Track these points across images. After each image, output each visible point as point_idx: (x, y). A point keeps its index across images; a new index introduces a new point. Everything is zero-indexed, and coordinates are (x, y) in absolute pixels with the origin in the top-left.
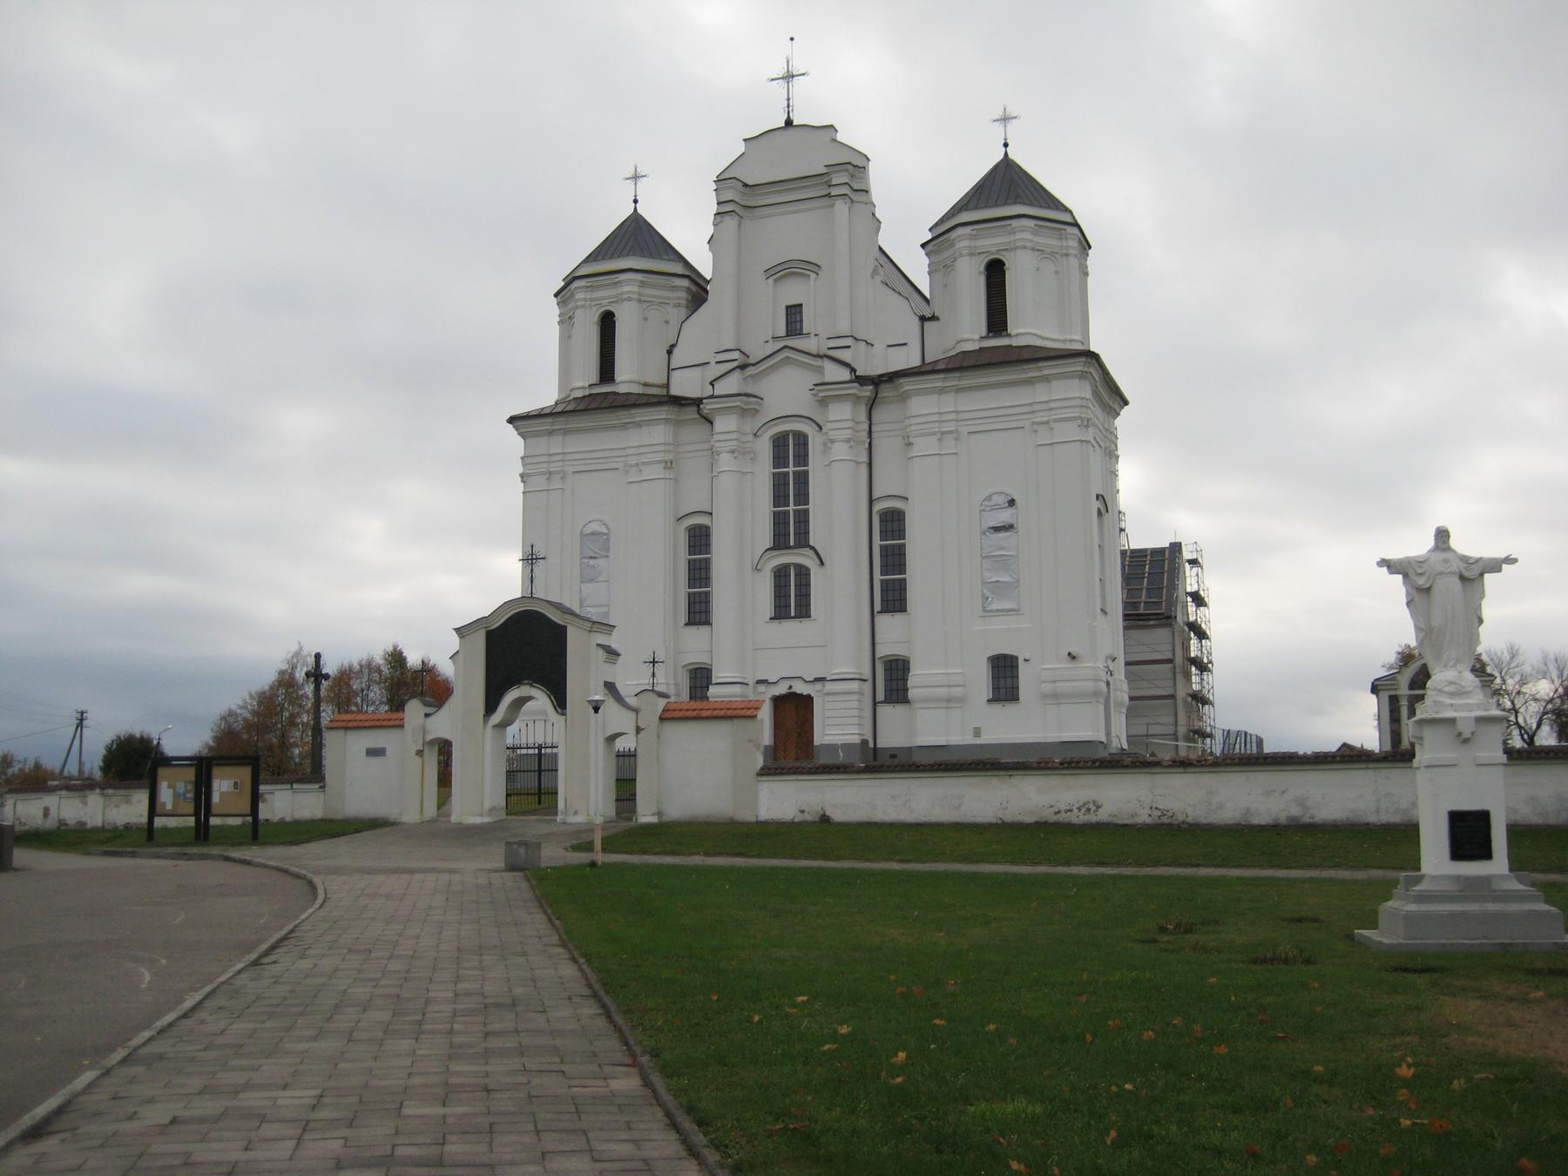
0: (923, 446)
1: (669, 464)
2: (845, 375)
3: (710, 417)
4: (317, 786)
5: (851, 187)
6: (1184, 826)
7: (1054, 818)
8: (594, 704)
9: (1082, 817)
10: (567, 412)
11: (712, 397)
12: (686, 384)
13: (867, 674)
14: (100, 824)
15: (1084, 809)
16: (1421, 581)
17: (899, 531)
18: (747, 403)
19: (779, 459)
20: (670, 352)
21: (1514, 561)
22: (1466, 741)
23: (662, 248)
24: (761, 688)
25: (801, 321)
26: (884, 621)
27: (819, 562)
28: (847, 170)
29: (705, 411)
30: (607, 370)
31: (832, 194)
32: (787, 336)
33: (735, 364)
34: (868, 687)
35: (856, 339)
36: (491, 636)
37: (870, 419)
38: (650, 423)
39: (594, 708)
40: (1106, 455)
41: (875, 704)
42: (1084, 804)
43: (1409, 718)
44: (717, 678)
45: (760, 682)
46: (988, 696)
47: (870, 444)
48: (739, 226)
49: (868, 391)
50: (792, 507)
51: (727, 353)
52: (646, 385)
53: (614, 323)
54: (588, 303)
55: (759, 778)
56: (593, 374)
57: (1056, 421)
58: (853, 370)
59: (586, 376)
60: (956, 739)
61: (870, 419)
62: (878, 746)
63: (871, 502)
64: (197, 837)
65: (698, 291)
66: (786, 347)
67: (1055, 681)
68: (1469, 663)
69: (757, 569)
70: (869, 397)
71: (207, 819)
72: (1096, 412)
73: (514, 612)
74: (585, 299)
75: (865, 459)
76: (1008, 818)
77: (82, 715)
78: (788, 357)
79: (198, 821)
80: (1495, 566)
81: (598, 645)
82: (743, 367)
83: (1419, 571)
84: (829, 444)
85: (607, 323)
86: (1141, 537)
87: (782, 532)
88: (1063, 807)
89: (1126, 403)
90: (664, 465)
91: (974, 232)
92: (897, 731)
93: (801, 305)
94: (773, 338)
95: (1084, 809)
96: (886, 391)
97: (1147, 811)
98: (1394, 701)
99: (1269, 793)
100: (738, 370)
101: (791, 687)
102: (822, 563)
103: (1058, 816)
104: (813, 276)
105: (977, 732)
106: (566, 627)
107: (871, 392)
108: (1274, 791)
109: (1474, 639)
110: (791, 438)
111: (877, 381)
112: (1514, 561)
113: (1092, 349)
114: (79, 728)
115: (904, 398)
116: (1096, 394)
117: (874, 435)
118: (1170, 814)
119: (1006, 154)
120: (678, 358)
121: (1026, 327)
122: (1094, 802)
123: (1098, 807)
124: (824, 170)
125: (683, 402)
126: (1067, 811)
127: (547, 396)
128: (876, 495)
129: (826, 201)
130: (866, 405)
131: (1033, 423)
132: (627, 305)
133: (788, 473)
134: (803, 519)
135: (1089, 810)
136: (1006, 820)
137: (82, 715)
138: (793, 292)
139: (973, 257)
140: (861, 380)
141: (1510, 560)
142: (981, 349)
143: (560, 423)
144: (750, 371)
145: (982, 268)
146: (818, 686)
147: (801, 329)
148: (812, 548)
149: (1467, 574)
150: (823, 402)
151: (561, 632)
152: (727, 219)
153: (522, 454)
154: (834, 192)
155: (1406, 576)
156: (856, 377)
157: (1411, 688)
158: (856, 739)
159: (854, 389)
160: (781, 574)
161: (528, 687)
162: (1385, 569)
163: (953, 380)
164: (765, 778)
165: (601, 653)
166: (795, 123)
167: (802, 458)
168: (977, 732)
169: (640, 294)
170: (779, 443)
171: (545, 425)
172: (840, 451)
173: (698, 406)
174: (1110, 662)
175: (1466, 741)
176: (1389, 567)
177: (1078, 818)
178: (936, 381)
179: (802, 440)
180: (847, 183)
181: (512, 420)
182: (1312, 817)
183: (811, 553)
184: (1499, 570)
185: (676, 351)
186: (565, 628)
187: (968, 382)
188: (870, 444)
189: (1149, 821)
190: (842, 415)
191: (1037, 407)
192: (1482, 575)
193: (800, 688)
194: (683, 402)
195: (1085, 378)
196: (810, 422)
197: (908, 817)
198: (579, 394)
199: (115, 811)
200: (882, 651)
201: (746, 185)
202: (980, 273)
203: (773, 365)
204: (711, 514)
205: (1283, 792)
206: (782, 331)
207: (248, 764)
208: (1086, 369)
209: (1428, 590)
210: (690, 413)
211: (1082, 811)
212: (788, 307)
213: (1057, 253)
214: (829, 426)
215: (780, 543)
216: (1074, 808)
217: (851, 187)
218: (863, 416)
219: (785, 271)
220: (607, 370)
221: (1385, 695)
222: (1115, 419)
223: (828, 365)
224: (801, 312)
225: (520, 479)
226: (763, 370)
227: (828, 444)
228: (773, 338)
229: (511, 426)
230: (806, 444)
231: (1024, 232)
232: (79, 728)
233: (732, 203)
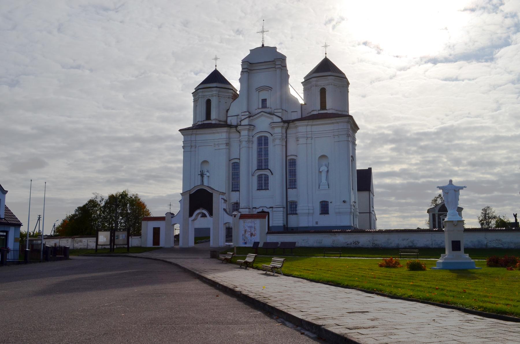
0: (302, 141)
1: (227, 144)
2: (280, 120)
3: (240, 131)
4: (139, 237)
5: (281, 65)
6: (382, 248)
7: (346, 246)
8: (234, 215)
9: (354, 246)
10: (193, 129)
11: (240, 125)
12: (232, 121)
13: (285, 206)
14: (72, 248)
15: (355, 244)
16: (446, 191)
17: (294, 165)
18: (251, 127)
19: (259, 144)
20: (227, 111)
21: (466, 187)
22: (456, 226)
23: (223, 80)
24: (254, 210)
25: (266, 104)
26: (290, 191)
27: (271, 174)
28: (281, 61)
29: (238, 129)
30: (208, 115)
31: (276, 67)
32: (262, 108)
33: (247, 116)
34: (285, 209)
35: (282, 110)
36: (190, 195)
37: (286, 133)
38: (221, 132)
39: (234, 216)
40: (353, 144)
41: (287, 214)
42: (355, 242)
43: (443, 221)
44: (241, 207)
45: (254, 208)
46: (320, 212)
47: (286, 140)
48: (248, 75)
49: (286, 125)
50: (263, 158)
51: (245, 113)
52: (220, 121)
53: (211, 102)
54: (203, 96)
55: (267, 235)
56: (204, 118)
57: (340, 135)
58: (282, 119)
59: (202, 118)
60: (311, 225)
61: (286, 133)
62: (288, 227)
63: (286, 156)
64: (111, 251)
65: (235, 96)
66: (262, 111)
67: (339, 209)
68: (456, 209)
69: (253, 175)
70: (286, 127)
71: (114, 247)
72: (351, 132)
73: (197, 189)
74: (202, 95)
75: (284, 144)
76: (334, 246)
77: (40, 217)
78: (262, 114)
79: (111, 247)
80: (462, 188)
81: (222, 198)
82: (249, 117)
83: (446, 189)
84: (274, 140)
85: (208, 102)
86: (360, 166)
87: (260, 165)
88: (349, 243)
89: (359, 129)
90: (226, 145)
91: (317, 80)
92: (294, 222)
93: (266, 99)
94: (258, 108)
95: (355, 244)
96: (291, 125)
97: (372, 244)
98: (434, 215)
99: (404, 240)
100: (248, 118)
101: (263, 209)
102: (272, 174)
103: (348, 245)
104: (270, 91)
105: (317, 223)
106: (213, 193)
107: (287, 125)
108: (405, 239)
109: (457, 204)
110: (263, 137)
111: (288, 122)
112: (466, 187)
113: (350, 114)
114: (39, 221)
115: (296, 127)
116: (351, 127)
117: (288, 138)
118: (378, 245)
119: (326, 57)
120: (230, 113)
121: (331, 105)
122: (357, 242)
123: (359, 243)
124: (274, 60)
125: (232, 127)
126: (350, 244)
127: (189, 124)
128: (288, 154)
129: (274, 69)
130: (285, 129)
131: (334, 135)
132: (215, 97)
133: (262, 148)
134: (267, 161)
135: (356, 244)
136: (334, 246)
137: (40, 217)
138: (264, 95)
139: (317, 87)
140: (284, 122)
141: (465, 187)
142: (319, 113)
143: (195, 131)
144: (251, 118)
145: (319, 90)
146: (271, 209)
147: (266, 106)
148: (269, 170)
149: (456, 190)
150: (273, 128)
151: (211, 195)
152: (245, 73)
153: (183, 141)
154: (277, 67)
155: (443, 190)
156: (283, 121)
157: (439, 211)
158: (282, 225)
159: (282, 124)
160: (260, 177)
161: (202, 210)
162: (438, 188)
163: (311, 122)
164: (268, 235)
165: (223, 201)
166: (264, 46)
167: (266, 144)
168: (317, 223)
169: (218, 94)
170: (260, 139)
171: (190, 132)
172: (278, 142)
173: (236, 128)
174: (354, 203)
175: (456, 226)
176: (439, 188)
177: (353, 246)
178: (305, 123)
179: (266, 138)
180: (280, 64)
181: (180, 130)
182: (415, 246)
183: (269, 171)
184: (463, 189)
185: (229, 111)
186: (212, 194)
187: (315, 123)
188: (286, 140)
189: (372, 247)
190: (278, 131)
191: (335, 131)
192: (459, 190)
193: (266, 210)
194: (232, 127)
195: (349, 123)
196: (268, 133)
197: (307, 245)
198: (200, 123)
199: (77, 244)
200: (290, 199)
201: (250, 63)
202: (318, 92)
203: (259, 116)
204: (240, 159)
205: (408, 239)
206: (260, 106)
207: (109, 231)
208: (349, 120)
209: (448, 193)
210: (234, 130)
211: (354, 244)
212: (262, 100)
213: (341, 86)
214: (275, 135)
215: (259, 168)
216: (352, 243)
217: (281, 65)
218: (284, 131)
219: (260, 89)
220: (208, 115)
221: (431, 213)
222: (355, 133)
223: (275, 117)
224: (266, 101)
225: (182, 148)
226: (256, 118)
227: (274, 140)
228: (258, 108)
229: (180, 132)
230: (268, 140)
231: (331, 80)
232: (39, 221)
233: (246, 69)
